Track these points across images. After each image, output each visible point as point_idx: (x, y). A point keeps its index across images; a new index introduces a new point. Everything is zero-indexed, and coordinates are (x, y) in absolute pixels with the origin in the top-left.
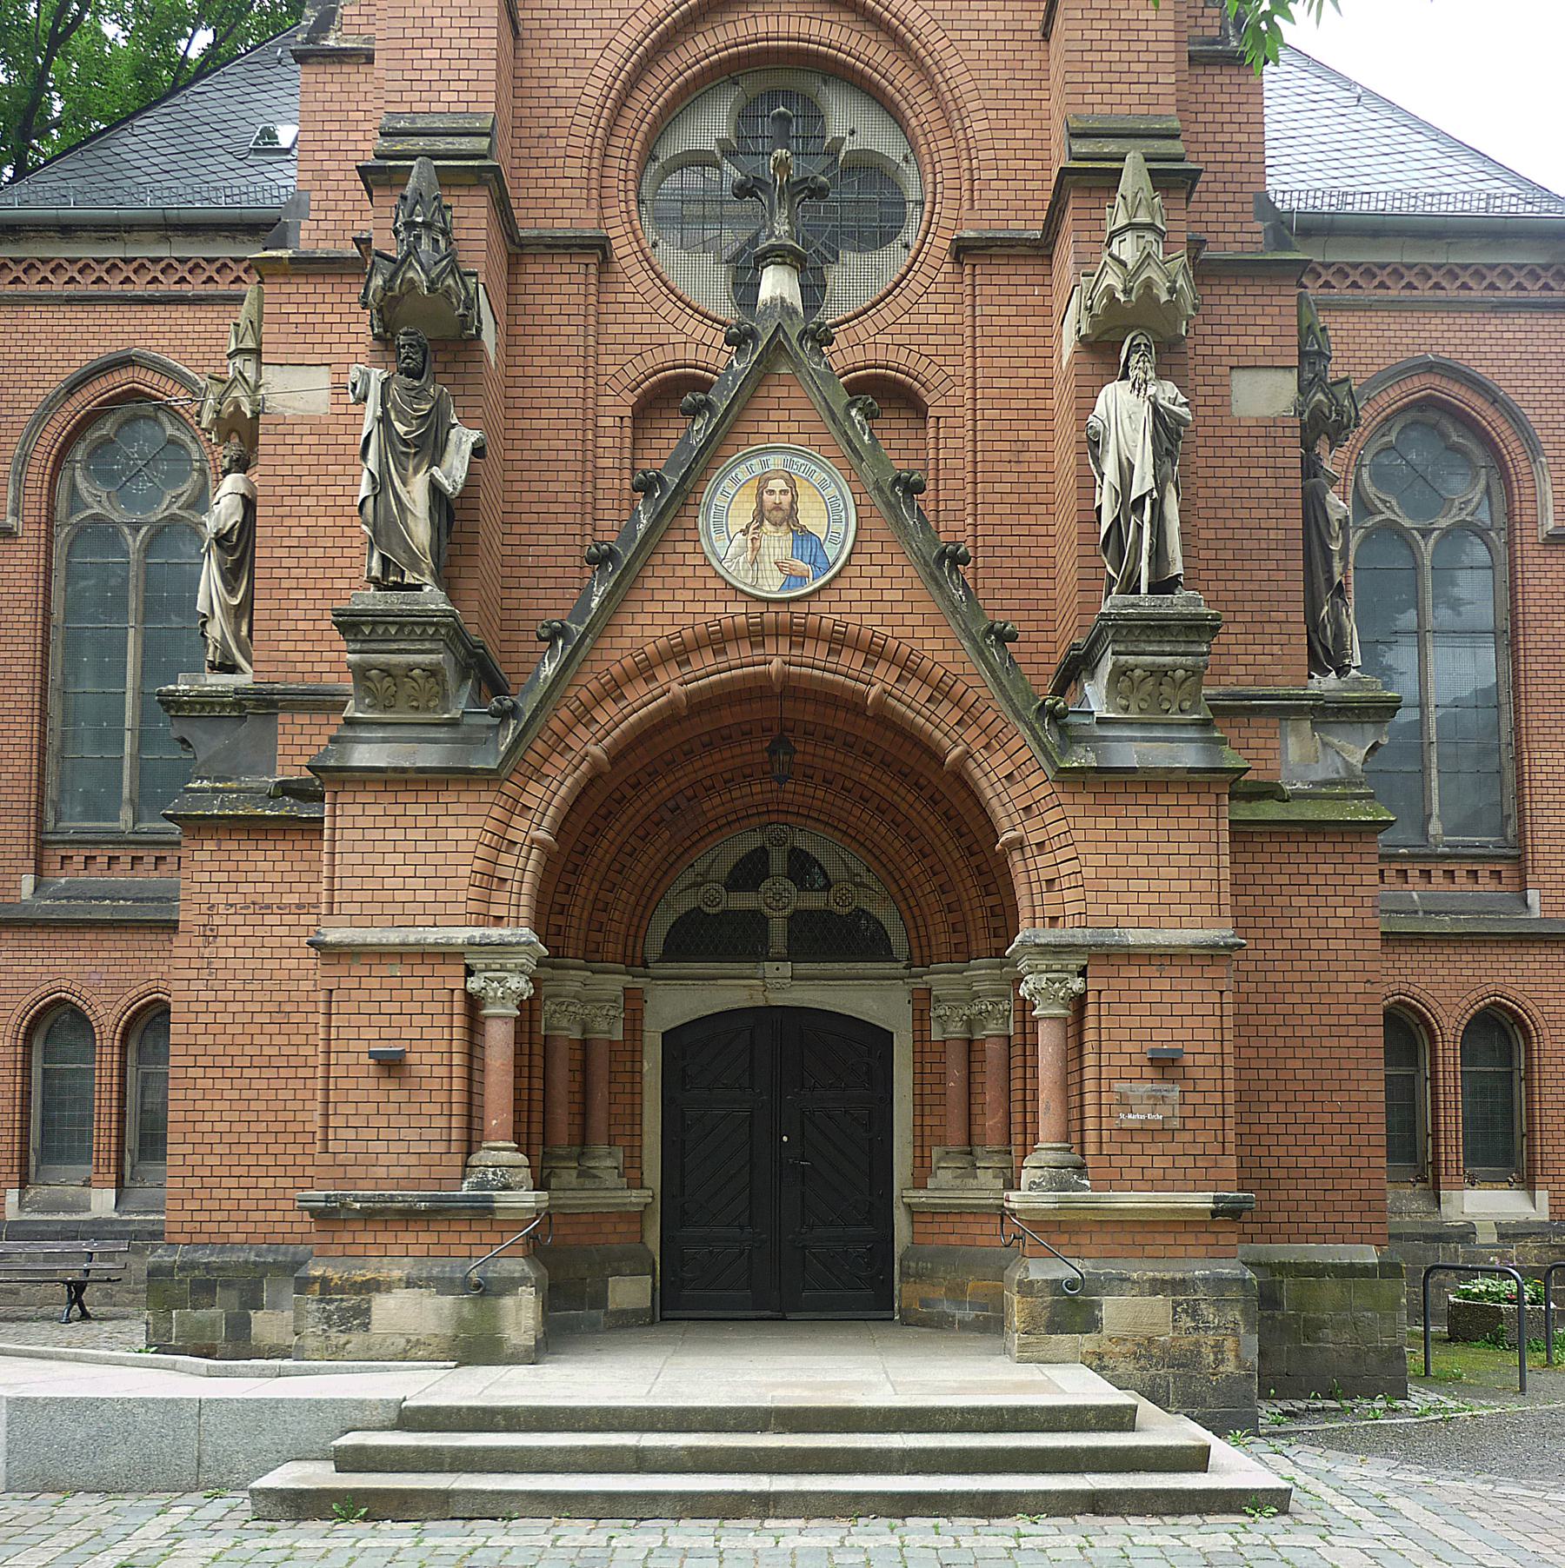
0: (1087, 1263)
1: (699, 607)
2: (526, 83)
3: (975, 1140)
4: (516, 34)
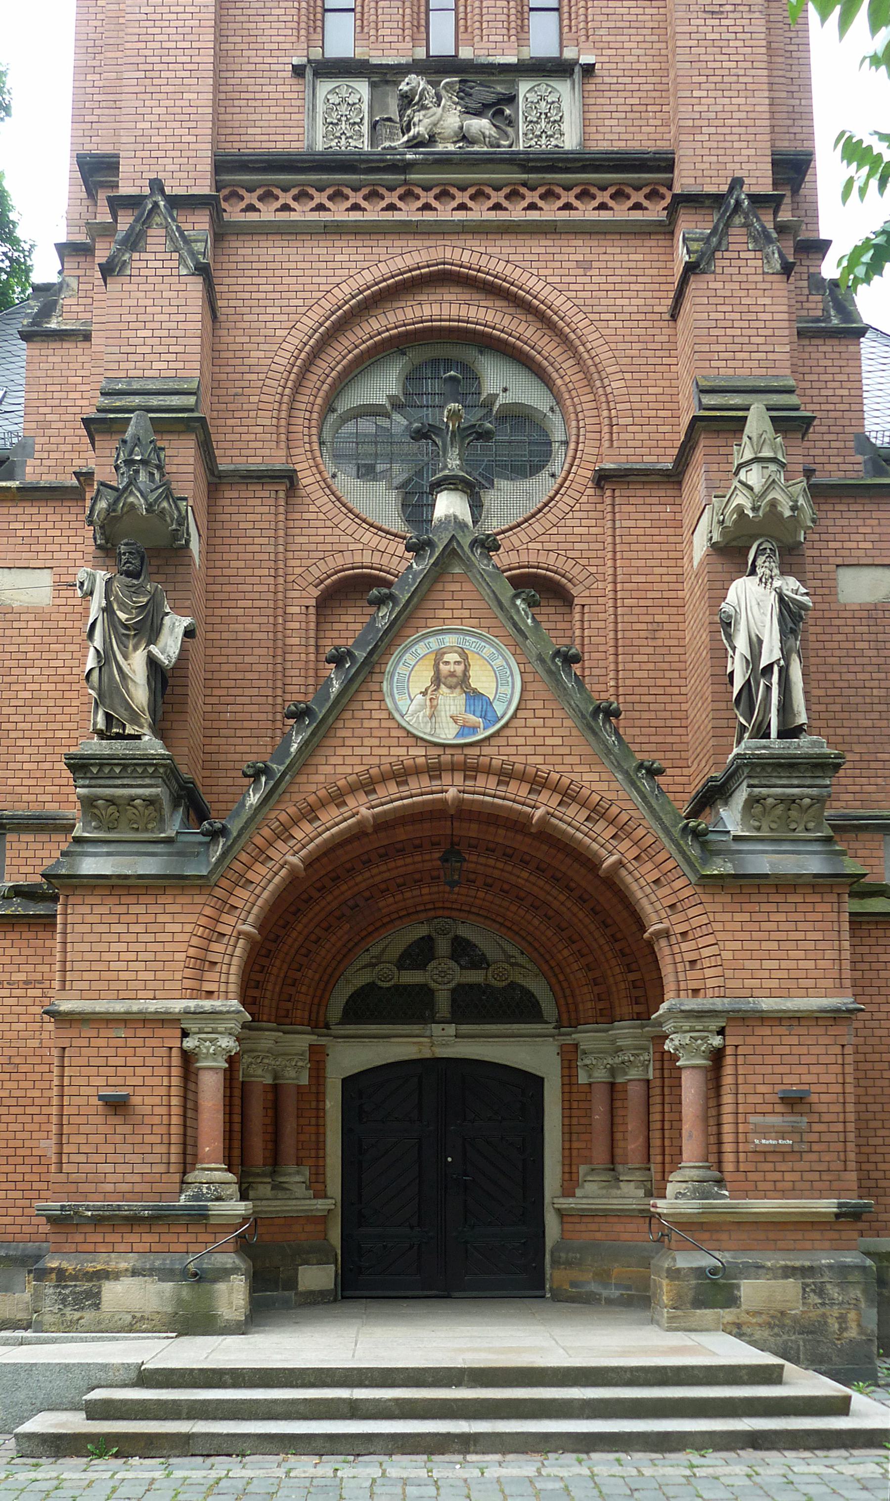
0: (727, 1254)
1: (384, 751)
2: (223, 355)
3: (618, 1159)
4: (214, 317)
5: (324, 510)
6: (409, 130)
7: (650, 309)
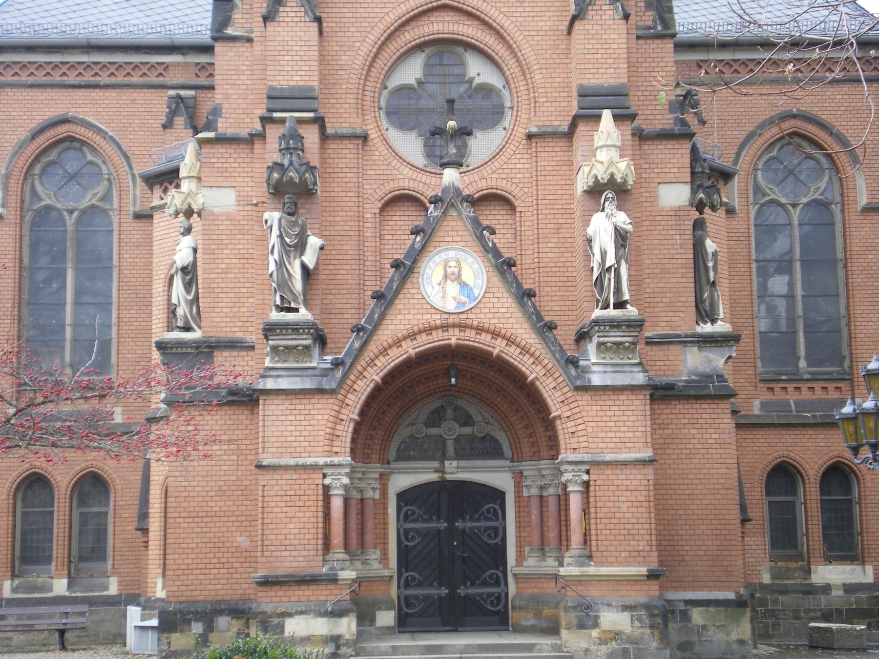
1: (420, 317)
2: (327, 58)
3: (546, 543)
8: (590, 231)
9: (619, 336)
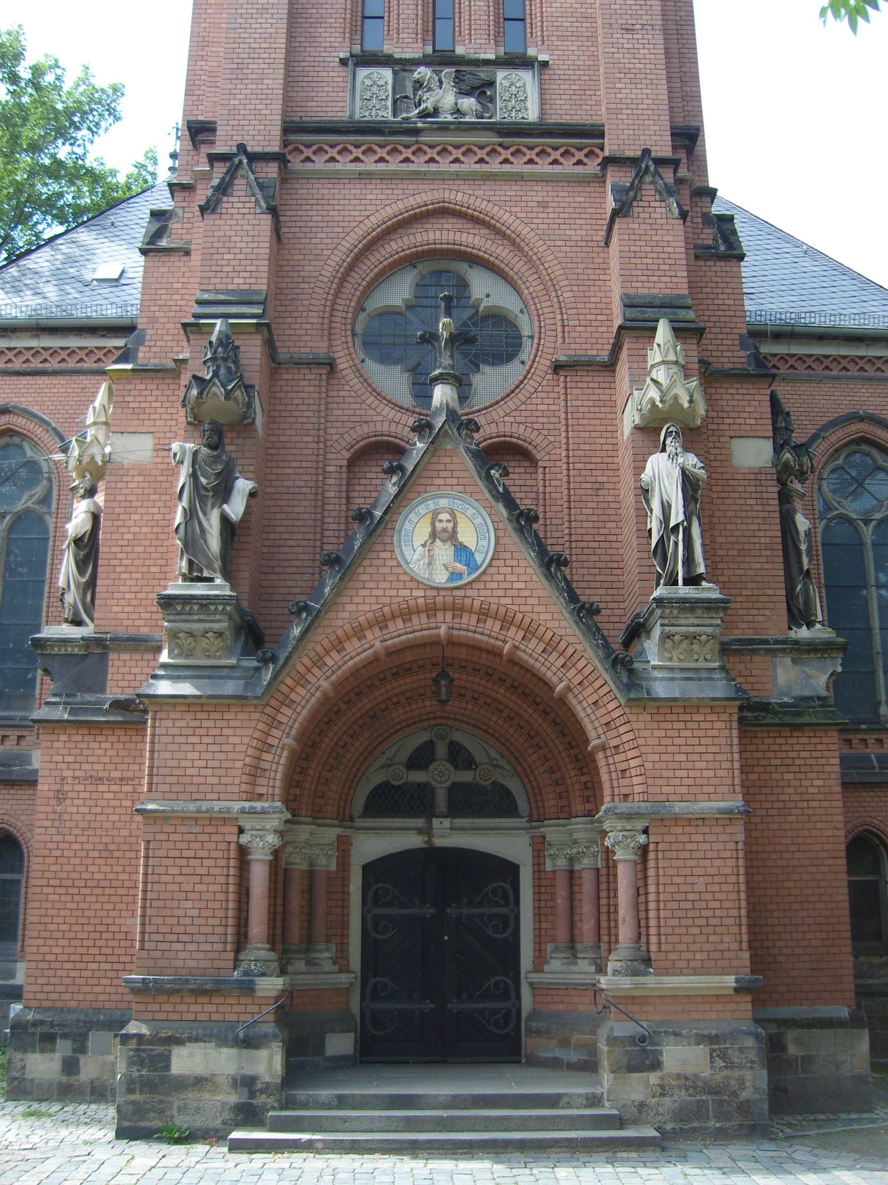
1: (393, 593)
2: (285, 269)
3: (577, 938)
5: (355, 389)
6: (420, 105)
7: (590, 238)
8: (646, 476)
9: (693, 625)
